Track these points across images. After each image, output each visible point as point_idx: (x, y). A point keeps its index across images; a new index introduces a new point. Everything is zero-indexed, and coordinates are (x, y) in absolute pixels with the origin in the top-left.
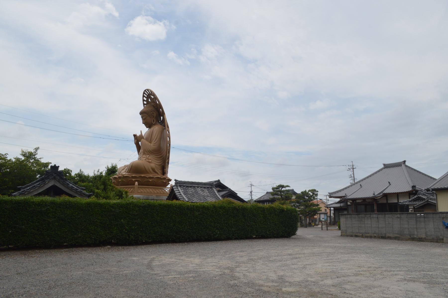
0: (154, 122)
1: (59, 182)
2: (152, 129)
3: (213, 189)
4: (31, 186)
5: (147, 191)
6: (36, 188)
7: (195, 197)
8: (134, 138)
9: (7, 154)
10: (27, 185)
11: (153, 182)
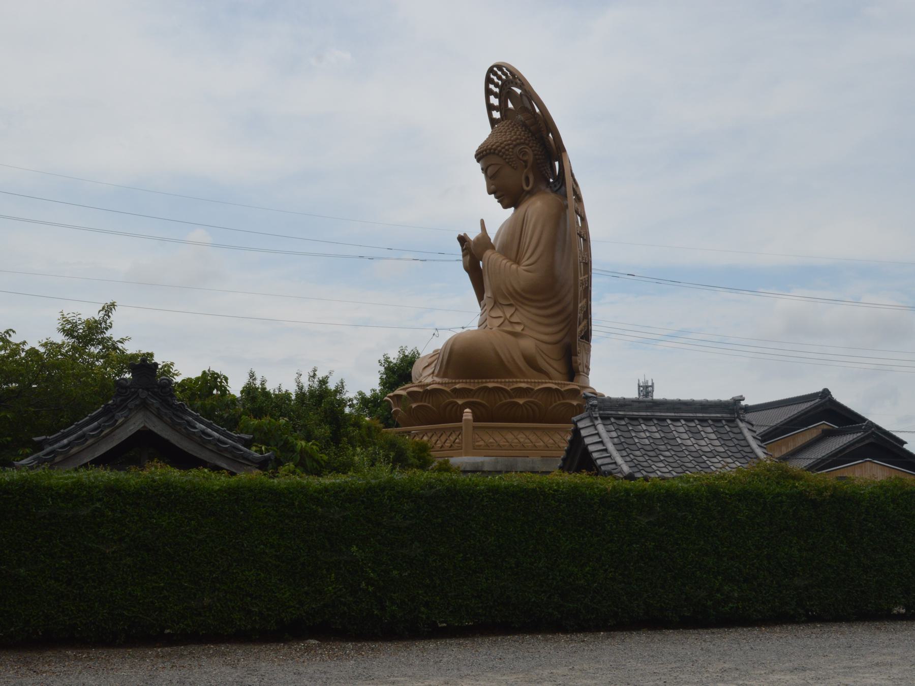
0: (528, 185)
1: (160, 417)
2: (522, 208)
3: (737, 426)
4: (75, 436)
5: (508, 442)
6: (87, 440)
7: (662, 458)
8: (463, 250)
9: (11, 330)
10: (62, 431)
11: (530, 407)
